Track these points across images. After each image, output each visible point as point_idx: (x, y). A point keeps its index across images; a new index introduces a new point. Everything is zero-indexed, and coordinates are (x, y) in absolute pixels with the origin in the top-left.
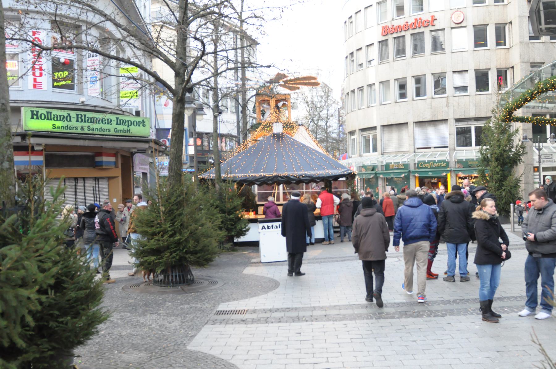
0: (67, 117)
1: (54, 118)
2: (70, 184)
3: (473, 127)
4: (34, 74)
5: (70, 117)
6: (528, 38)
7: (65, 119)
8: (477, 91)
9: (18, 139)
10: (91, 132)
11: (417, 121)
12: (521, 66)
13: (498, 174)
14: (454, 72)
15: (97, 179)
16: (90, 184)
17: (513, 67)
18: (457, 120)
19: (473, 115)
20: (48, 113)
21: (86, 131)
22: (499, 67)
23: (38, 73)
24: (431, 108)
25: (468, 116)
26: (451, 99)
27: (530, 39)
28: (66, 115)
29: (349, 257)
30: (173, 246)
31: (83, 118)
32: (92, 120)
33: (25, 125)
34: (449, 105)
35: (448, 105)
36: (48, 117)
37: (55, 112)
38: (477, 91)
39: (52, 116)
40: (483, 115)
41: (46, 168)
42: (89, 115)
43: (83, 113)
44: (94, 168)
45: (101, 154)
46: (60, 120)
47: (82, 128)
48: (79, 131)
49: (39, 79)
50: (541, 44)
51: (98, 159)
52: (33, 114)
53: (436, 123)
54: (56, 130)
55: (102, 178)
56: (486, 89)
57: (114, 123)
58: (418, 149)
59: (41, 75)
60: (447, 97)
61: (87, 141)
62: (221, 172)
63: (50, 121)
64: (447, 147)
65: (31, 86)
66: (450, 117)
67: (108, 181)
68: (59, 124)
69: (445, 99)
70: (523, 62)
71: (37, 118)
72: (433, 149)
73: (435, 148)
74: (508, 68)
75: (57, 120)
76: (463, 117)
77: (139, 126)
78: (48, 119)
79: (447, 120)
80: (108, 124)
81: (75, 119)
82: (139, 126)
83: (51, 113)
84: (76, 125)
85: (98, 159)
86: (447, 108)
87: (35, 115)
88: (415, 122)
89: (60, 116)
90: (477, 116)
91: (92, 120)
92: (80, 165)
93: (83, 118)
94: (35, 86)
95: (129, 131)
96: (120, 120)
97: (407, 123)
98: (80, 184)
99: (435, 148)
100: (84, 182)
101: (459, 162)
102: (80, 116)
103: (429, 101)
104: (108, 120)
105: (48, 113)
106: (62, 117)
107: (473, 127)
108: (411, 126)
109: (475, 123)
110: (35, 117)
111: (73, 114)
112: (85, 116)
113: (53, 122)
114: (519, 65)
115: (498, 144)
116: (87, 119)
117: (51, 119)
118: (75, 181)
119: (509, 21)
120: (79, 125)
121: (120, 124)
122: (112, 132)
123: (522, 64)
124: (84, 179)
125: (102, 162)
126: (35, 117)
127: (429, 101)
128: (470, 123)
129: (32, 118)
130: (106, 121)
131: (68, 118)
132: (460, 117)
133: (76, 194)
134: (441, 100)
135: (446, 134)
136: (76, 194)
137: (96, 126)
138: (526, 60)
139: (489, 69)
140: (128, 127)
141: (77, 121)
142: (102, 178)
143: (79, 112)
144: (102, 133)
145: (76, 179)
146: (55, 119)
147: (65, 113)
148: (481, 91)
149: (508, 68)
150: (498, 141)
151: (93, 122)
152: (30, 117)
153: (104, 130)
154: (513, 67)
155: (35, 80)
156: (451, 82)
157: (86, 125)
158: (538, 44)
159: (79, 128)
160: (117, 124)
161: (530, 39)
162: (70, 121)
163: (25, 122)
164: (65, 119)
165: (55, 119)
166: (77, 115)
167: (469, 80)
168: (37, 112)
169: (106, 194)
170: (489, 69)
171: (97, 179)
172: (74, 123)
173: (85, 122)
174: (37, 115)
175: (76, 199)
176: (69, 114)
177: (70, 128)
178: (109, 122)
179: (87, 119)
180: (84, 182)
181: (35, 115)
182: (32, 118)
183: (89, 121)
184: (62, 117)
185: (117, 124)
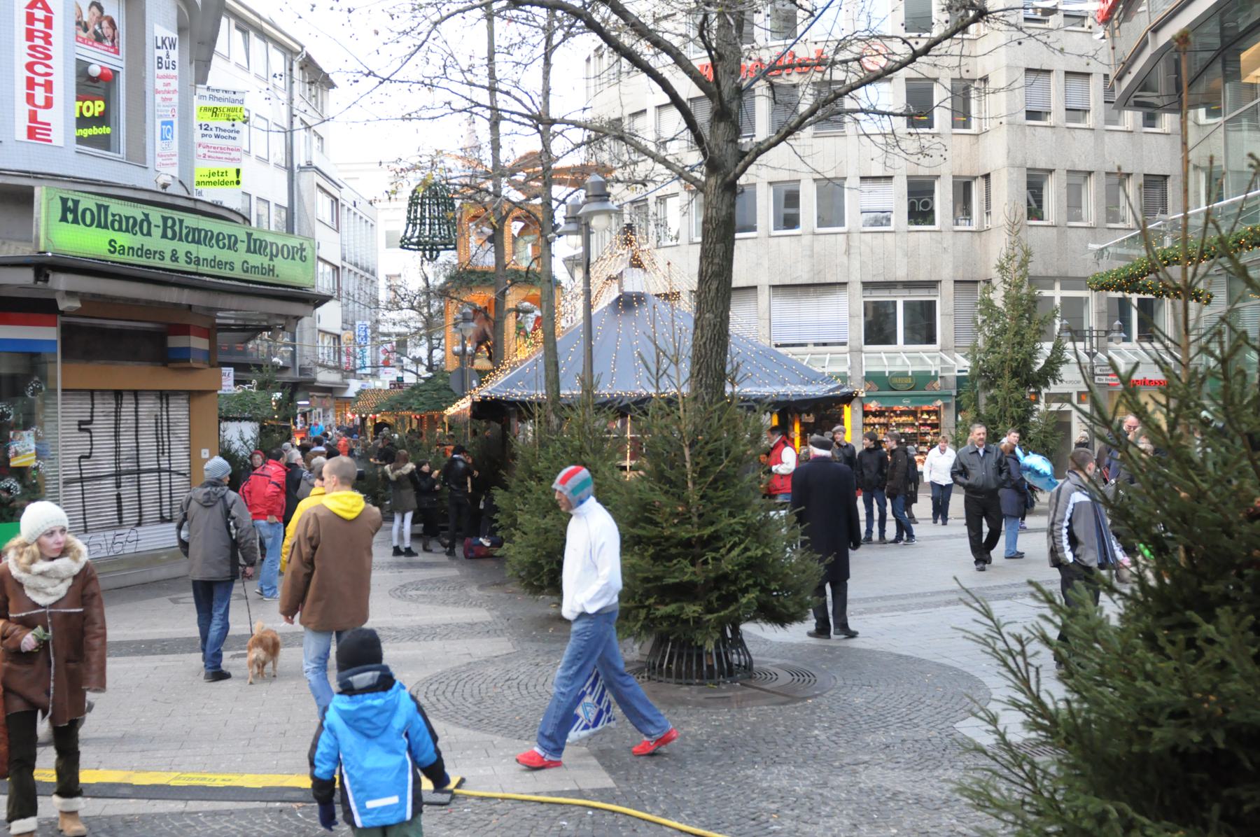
0: (142, 221)
1: (113, 222)
2: (104, 407)
3: (900, 300)
4: (30, 99)
5: (149, 224)
6: (1024, 115)
7: (137, 228)
8: (910, 223)
9: (25, 277)
10: (192, 268)
11: (778, 283)
12: (1010, 174)
13: (1019, 407)
14: (862, 178)
15: (164, 396)
16: (148, 407)
17: (987, 177)
18: (867, 285)
19: (901, 275)
20: (99, 206)
21: (182, 265)
22: (957, 173)
23: (40, 94)
24: (812, 256)
25: (890, 278)
26: (855, 237)
27: (1027, 118)
28: (140, 217)
29: (933, 594)
30: (743, 576)
31: (177, 228)
32: (197, 237)
33: (47, 238)
34: (852, 251)
35: (848, 252)
36: (101, 220)
37: (116, 207)
38: (910, 223)
39: (110, 218)
40: (922, 276)
41: (63, 362)
42: (191, 221)
43: (177, 215)
44: (165, 365)
45: (184, 330)
46: (127, 230)
47: (174, 257)
48: (168, 263)
49: (43, 115)
50: (1049, 130)
51: (175, 342)
52: (65, 210)
53: (821, 289)
54: (116, 257)
55: (177, 393)
56: (929, 219)
57: (242, 247)
58: (777, 346)
59: (49, 104)
60: (848, 233)
61: (186, 292)
62: (562, 385)
63: (105, 231)
64: (844, 344)
65: (22, 134)
66: (852, 278)
67: (189, 401)
68: (123, 239)
69: (841, 238)
70: (1013, 166)
71: (75, 221)
72: (811, 348)
73: (816, 345)
74: (975, 178)
75: (120, 229)
76: (881, 279)
77: (293, 258)
78: (99, 226)
79: (845, 284)
80: (229, 248)
81: (160, 231)
82: (293, 258)
83: (106, 208)
84: (163, 249)
85: (175, 342)
86: (845, 257)
87: (71, 211)
88: (774, 287)
89: (127, 219)
90: (910, 279)
91: (197, 237)
92: (133, 356)
93: (177, 228)
94: (31, 133)
95: (273, 270)
96: (255, 241)
97: (755, 287)
98: (128, 408)
99: (816, 345)
100: (137, 404)
101: (870, 377)
102: (170, 223)
103: (806, 240)
104: (230, 237)
105: (99, 206)
106: (131, 221)
107: (900, 300)
108: (764, 295)
109: (906, 292)
110: (70, 217)
111: (156, 215)
112: (181, 221)
113: (111, 234)
114: (1004, 173)
115: (1018, 339)
116: (184, 231)
117: (106, 227)
118: (117, 400)
119: (980, 75)
120: (167, 246)
121: (255, 252)
122: (237, 272)
123: (1012, 170)
124: (136, 394)
125: (188, 349)
126: (70, 217)
127: (806, 240)
128: (894, 292)
129: (64, 219)
130: (226, 241)
131: (145, 224)
132: (875, 280)
133: (117, 434)
134: (832, 240)
135: (842, 314)
136: (117, 434)
137: (204, 252)
138: (1018, 162)
139: (938, 177)
140: (271, 259)
141: (164, 236)
142: (177, 393)
143: (168, 213)
144: (216, 271)
145: (118, 395)
146: (116, 225)
147: (137, 212)
148: (917, 224)
149: (975, 178)
150: (1016, 334)
151: (199, 242)
152: (59, 215)
153: (220, 263)
154: (987, 177)
155: (33, 117)
156: (856, 201)
157: (182, 247)
158: (1043, 130)
159: (168, 255)
160: (249, 250)
161: (1027, 118)
162: (149, 234)
163: (47, 234)
164: (137, 228)
165: (116, 225)
166: (165, 219)
167: (895, 199)
168: (76, 203)
169: (184, 435)
170: (938, 177)
171: (164, 396)
172: (155, 242)
173: (181, 239)
174: (74, 211)
175: (117, 447)
176: (146, 215)
177: (148, 253)
178: (232, 244)
179: (184, 231)
180: (137, 404)
181: (70, 212)
182: (64, 219)
183: (190, 239)
184: (131, 221)
185: (249, 250)
